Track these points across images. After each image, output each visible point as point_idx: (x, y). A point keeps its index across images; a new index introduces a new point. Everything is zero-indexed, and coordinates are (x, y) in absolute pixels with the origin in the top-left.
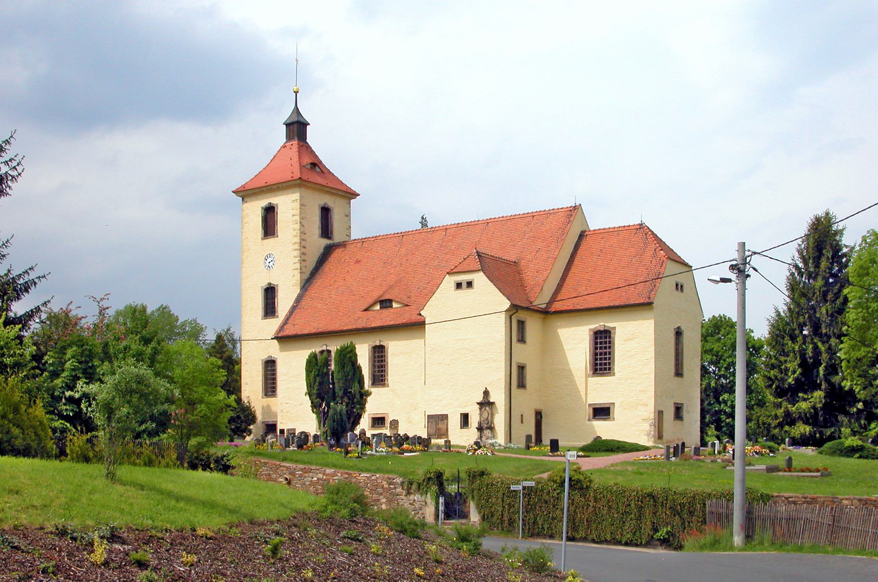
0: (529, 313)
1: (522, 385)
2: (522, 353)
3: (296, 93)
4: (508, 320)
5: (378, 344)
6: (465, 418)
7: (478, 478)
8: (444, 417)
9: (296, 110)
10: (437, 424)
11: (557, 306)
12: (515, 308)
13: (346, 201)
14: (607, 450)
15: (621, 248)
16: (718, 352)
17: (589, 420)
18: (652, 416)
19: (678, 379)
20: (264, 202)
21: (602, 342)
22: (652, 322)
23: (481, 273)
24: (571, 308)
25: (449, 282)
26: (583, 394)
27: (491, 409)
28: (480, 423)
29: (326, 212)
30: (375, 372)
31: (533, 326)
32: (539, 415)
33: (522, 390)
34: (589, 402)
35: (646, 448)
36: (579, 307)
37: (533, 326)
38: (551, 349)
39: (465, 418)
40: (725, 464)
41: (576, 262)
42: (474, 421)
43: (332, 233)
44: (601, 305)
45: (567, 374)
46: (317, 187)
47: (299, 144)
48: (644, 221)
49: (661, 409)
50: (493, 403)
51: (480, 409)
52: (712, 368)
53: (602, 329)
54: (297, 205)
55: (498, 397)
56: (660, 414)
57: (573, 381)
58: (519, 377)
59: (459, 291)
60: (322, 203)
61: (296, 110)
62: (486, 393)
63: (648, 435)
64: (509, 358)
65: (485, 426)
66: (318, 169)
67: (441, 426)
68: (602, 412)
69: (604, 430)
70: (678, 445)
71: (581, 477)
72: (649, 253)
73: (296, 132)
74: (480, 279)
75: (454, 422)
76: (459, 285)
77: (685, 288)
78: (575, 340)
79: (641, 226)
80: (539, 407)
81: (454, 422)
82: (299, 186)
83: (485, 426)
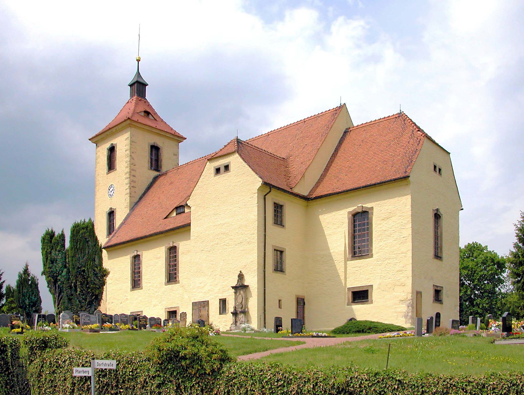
0: (292, 198)
1: (279, 268)
2: (278, 237)
3: (138, 61)
4: (262, 201)
5: (172, 246)
6: (223, 302)
7: (38, 352)
8: (205, 304)
9: (138, 73)
10: (200, 311)
11: (319, 192)
12: (268, 187)
13: (176, 143)
14: (359, 332)
15: (381, 135)
16: (472, 269)
17: (348, 305)
18: (410, 296)
19: (437, 261)
20: (108, 145)
21: (360, 223)
22: (409, 197)
23: (237, 155)
24: (330, 192)
25: (210, 167)
26: (342, 278)
27: (245, 292)
28: (235, 308)
29: (155, 149)
30: (170, 270)
31: (292, 211)
32: (301, 302)
33: (279, 275)
34: (349, 286)
35: (402, 329)
36: (338, 191)
37: (292, 211)
38: (313, 234)
39: (223, 302)
40: (492, 339)
41: (339, 154)
42: (230, 307)
43: (161, 167)
44: (359, 186)
45: (329, 258)
46: (146, 128)
47: (137, 99)
48: (402, 110)
49: (419, 290)
50: (247, 286)
51: (236, 293)
52: (467, 283)
53: (360, 211)
54: (128, 142)
55: (252, 280)
56: (418, 295)
57: (335, 270)
58: (276, 261)
59: (218, 176)
60: (152, 142)
61: (138, 73)
62: (241, 276)
63: (406, 316)
64: (263, 240)
65: (240, 310)
66: (150, 116)
67: (204, 313)
68: (361, 295)
69: (362, 312)
70: (432, 318)
71: (203, 352)
72: (407, 134)
73: (136, 90)
74: (235, 161)
75: (214, 307)
76: (218, 171)
77: (443, 171)
78: (335, 225)
79: (401, 116)
80: (301, 294)
81: (214, 307)
82: (130, 125)
83: (239, 310)
